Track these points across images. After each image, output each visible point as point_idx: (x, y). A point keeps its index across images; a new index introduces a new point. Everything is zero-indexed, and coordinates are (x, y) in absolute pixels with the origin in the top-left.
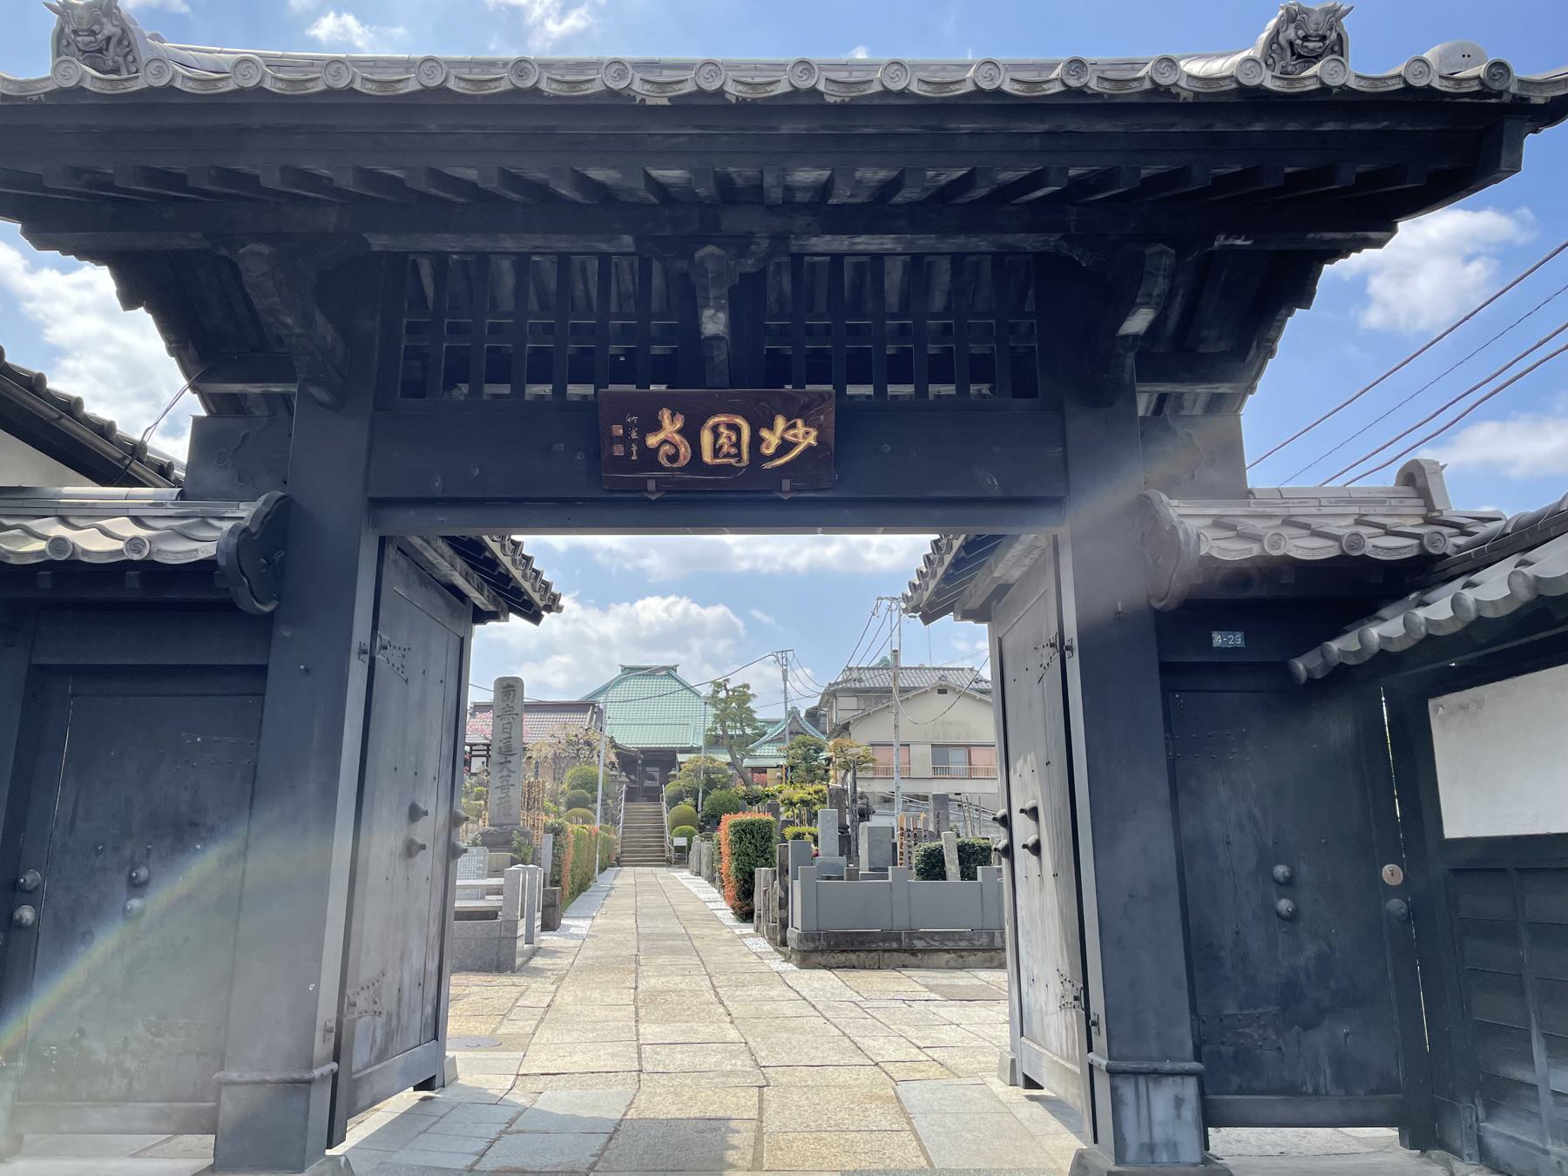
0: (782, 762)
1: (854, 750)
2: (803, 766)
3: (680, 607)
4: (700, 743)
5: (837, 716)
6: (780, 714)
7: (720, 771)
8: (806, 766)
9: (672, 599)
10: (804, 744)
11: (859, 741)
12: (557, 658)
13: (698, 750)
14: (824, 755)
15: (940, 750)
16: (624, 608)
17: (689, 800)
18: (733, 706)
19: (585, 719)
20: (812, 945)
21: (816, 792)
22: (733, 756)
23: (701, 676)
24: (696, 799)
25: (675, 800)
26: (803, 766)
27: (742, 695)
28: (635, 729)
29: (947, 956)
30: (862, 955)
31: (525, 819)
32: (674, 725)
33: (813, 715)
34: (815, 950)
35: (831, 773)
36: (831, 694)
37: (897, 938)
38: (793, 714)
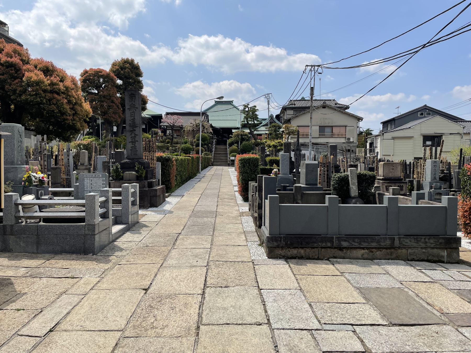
0: (267, 132)
1: (292, 128)
2: (274, 133)
3: (235, 84)
4: (239, 126)
5: (286, 117)
6: (266, 117)
7: (246, 135)
8: (275, 134)
9: (232, 81)
10: (275, 126)
11: (294, 125)
12: (197, 101)
13: (238, 128)
14: (282, 130)
15: (322, 128)
16: (216, 84)
17: (236, 145)
18: (250, 113)
19: (202, 118)
20: (275, 244)
21: (278, 143)
22: (250, 130)
23: (239, 103)
24: (238, 144)
25: (231, 145)
26: (274, 133)
27: (254, 110)
28: (219, 121)
29: (363, 251)
30: (308, 250)
31: (146, 157)
32: (232, 120)
33: (278, 117)
34: (278, 247)
35: (284, 136)
36: (284, 109)
37: (331, 240)
38: (271, 117)
